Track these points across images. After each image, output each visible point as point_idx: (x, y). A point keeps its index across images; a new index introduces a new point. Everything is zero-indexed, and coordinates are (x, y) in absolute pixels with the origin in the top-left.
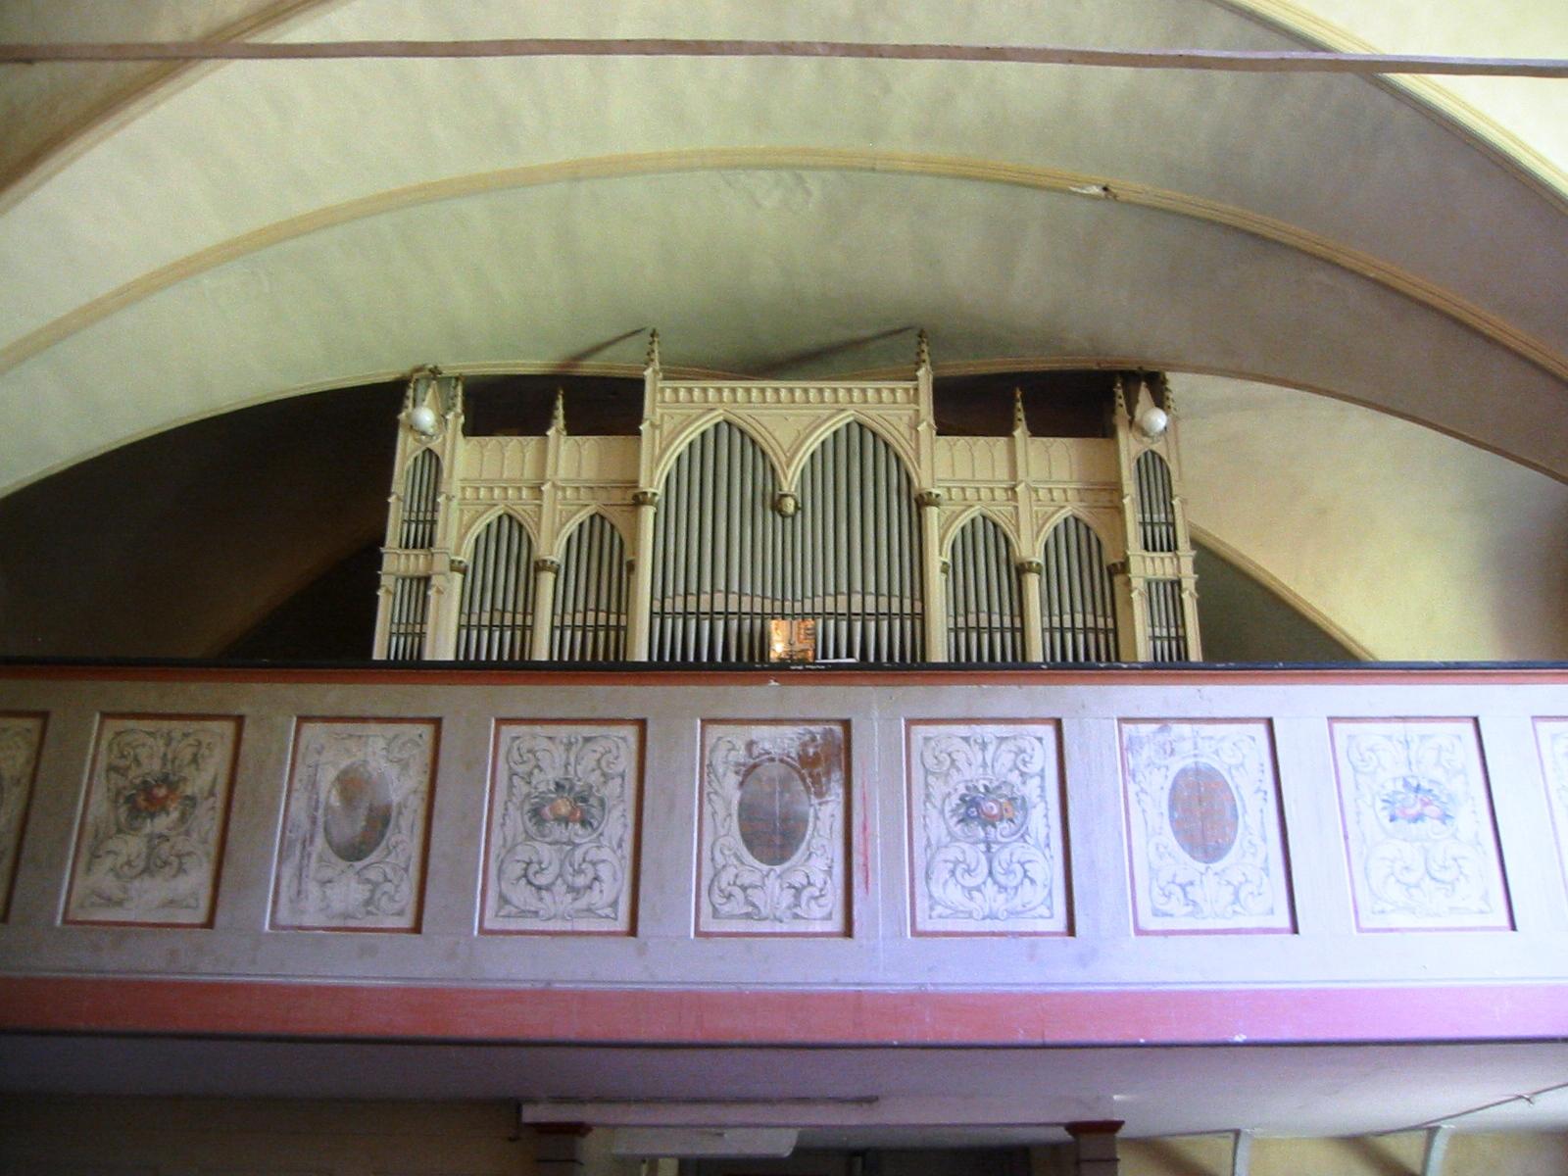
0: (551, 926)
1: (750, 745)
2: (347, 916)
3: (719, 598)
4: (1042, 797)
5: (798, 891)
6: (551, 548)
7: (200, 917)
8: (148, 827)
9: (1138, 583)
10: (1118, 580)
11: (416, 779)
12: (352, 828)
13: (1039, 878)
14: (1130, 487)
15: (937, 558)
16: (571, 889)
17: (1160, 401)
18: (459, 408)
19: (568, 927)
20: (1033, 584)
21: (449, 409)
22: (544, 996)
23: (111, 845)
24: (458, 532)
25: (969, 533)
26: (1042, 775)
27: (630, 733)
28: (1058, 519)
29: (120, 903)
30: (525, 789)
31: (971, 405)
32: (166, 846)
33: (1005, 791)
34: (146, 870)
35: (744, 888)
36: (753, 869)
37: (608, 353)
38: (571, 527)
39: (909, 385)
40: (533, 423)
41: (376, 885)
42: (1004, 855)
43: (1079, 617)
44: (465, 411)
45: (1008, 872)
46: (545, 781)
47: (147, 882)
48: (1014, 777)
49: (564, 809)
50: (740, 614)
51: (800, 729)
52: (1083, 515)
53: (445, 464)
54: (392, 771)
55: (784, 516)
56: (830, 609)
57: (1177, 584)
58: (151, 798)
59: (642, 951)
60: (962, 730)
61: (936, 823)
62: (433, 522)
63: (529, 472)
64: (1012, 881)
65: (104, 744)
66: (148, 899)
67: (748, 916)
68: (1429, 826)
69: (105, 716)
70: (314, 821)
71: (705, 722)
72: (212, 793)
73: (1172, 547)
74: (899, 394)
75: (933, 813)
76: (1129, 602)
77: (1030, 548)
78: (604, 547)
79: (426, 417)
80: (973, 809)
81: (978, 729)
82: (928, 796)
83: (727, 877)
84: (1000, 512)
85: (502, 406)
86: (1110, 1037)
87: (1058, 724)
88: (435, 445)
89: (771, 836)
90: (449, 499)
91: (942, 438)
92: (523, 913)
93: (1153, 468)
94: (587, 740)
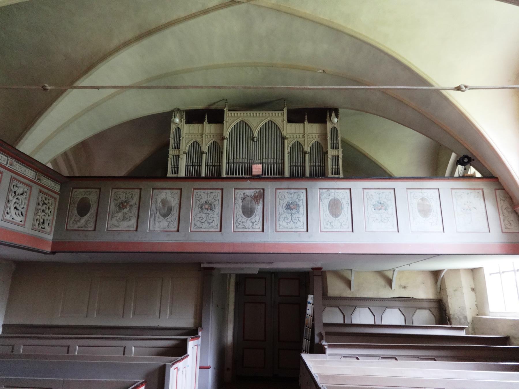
0: (204, 230)
1: (244, 194)
2: (164, 228)
3: (241, 160)
4: (303, 204)
5: (253, 223)
6: (205, 149)
7: (134, 229)
8: (123, 211)
9: (329, 156)
10: (326, 155)
11: (177, 201)
12: (165, 211)
13: (301, 221)
14: (329, 135)
15: (286, 151)
16: (208, 223)
17: (337, 116)
18: (184, 118)
19: (208, 230)
20: (307, 156)
21: (182, 118)
22: (203, 244)
23: (116, 215)
24: (185, 146)
25: (294, 145)
26: (303, 200)
27: (220, 191)
28: (313, 142)
29: (118, 227)
30: (199, 203)
31: (296, 116)
32: (127, 215)
33: (295, 203)
34: (123, 220)
35: (243, 222)
36: (244, 219)
37: (217, 104)
38: (209, 144)
39: (282, 112)
40: (200, 121)
41: (169, 222)
42: (294, 216)
43: (317, 163)
44: (186, 118)
45: (295, 220)
46: (203, 201)
47: (123, 222)
48: (297, 200)
49: (207, 206)
50: (245, 163)
51: (254, 190)
52: (319, 141)
53: (182, 131)
54: (172, 199)
55: (254, 142)
56: (264, 162)
57: (338, 156)
58: (123, 205)
59: (222, 235)
60: (287, 191)
61: (281, 210)
62: (180, 143)
63: (200, 132)
64: (296, 221)
65: (113, 195)
66: (124, 226)
67: (243, 228)
68: (382, 211)
69: (113, 188)
70: (157, 210)
71: (235, 189)
72: (136, 204)
73: (338, 148)
74: (280, 114)
75: (281, 207)
76: (328, 160)
77: (307, 149)
78: (216, 148)
79: (177, 120)
80: (288, 207)
81: (290, 190)
82: (280, 204)
83: (239, 220)
84: (301, 140)
85: (194, 116)
86: (314, 252)
87: (306, 189)
88: (179, 126)
89: (248, 212)
90: (183, 138)
91: (289, 124)
92: (199, 228)
93: (334, 130)
94: (211, 193)
